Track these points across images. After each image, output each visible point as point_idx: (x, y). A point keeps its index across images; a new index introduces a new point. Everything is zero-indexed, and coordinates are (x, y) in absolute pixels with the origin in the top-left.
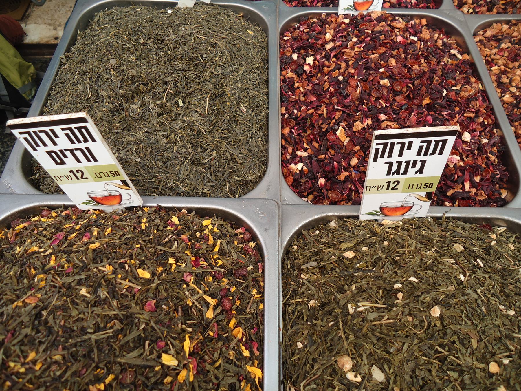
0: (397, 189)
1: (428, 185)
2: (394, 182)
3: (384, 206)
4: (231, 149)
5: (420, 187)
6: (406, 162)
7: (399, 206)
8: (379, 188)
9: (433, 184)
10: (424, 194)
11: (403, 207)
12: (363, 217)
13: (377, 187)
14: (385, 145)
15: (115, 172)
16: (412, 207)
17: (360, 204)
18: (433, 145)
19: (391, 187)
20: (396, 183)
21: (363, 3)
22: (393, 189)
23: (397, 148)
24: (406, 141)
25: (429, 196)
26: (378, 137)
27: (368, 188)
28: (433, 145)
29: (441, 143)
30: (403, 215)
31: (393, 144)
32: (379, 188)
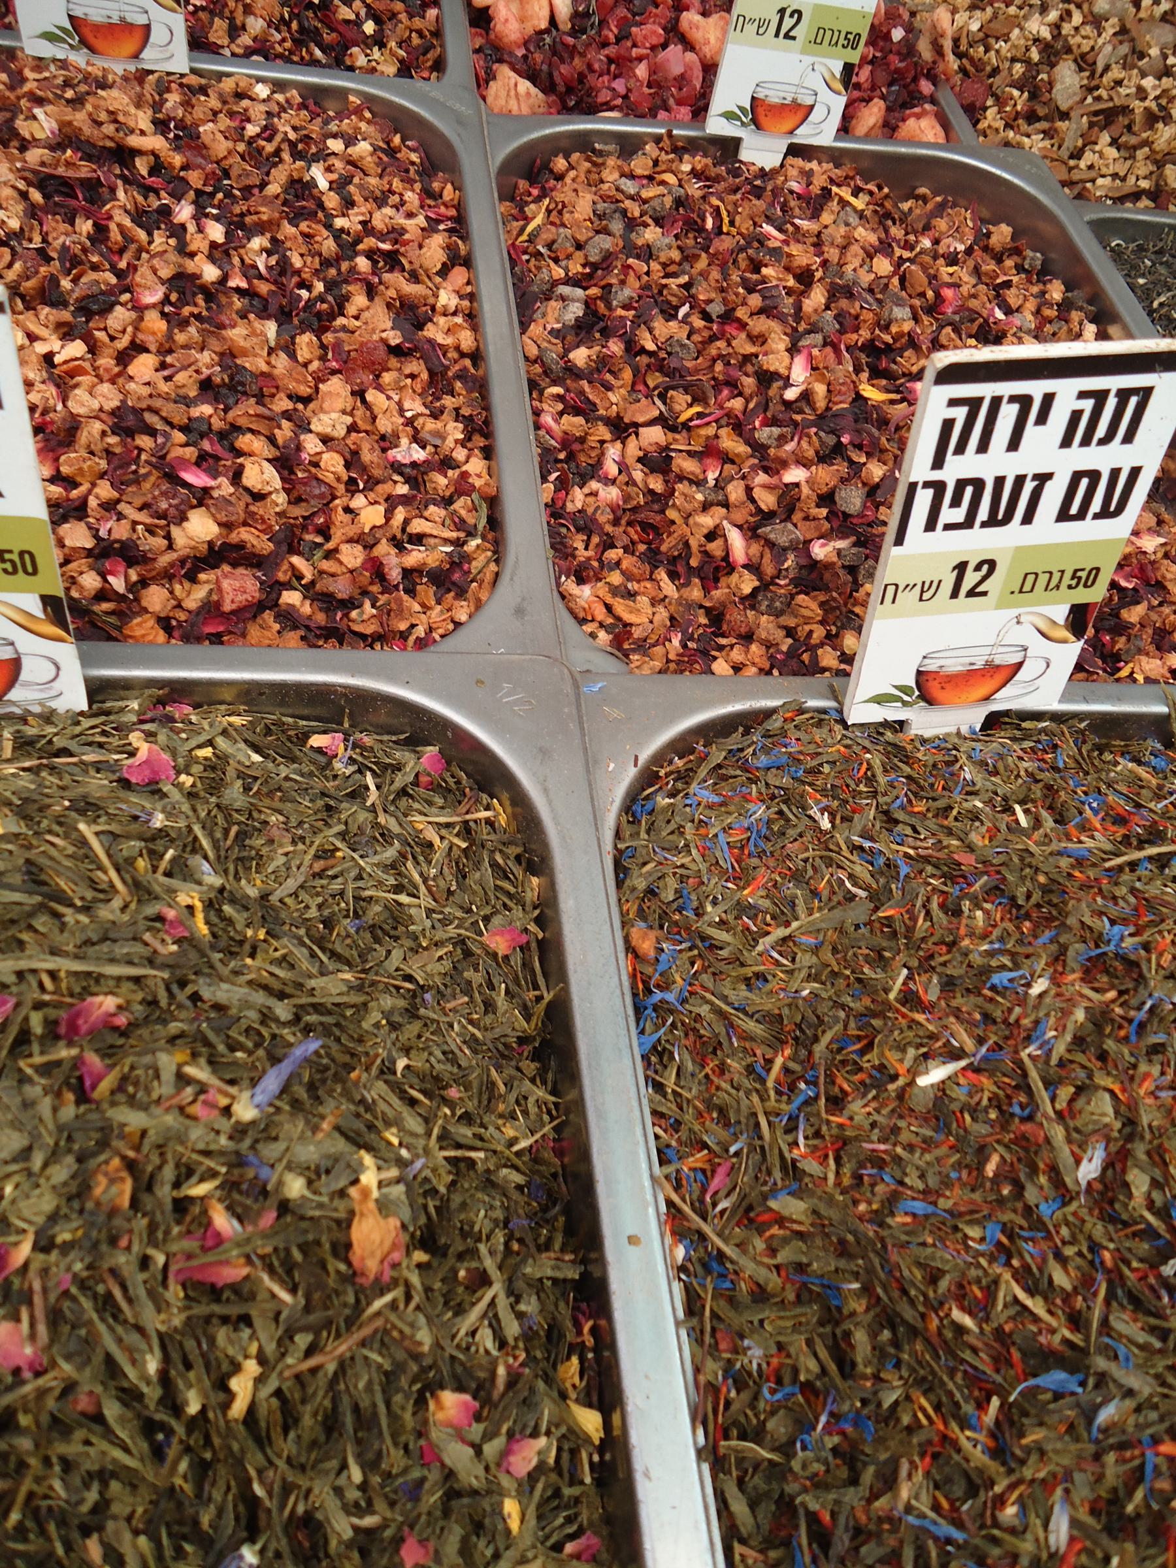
0: (985, 594)
1: (1083, 574)
2: (978, 568)
3: (932, 666)
4: (764, 943)
5: (1058, 587)
6: (1036, 477)
7: (980, 663)
8: (926, 591)
9: (1098, 569)
10: (1060, 613)
11: (991, 669)
12: (860, 713)
13: (918, 589)
14: (974, 404)
15: (22, 554)
16: (1019, 665)
17: (48, 500)
18: (1111, 403)
19: (966, 585)
20: (985, 567)
21: (783, 106)
22: (971, 593)
23: (1008, 414)
24: (1036, 388)
25: (1078, 618)
26: (950, 375)
27: (891, 589)
28: (1111, 403)
29: (1133, 401)
30: (987, 698)
31: (996, 402)
32: (926, 591)
